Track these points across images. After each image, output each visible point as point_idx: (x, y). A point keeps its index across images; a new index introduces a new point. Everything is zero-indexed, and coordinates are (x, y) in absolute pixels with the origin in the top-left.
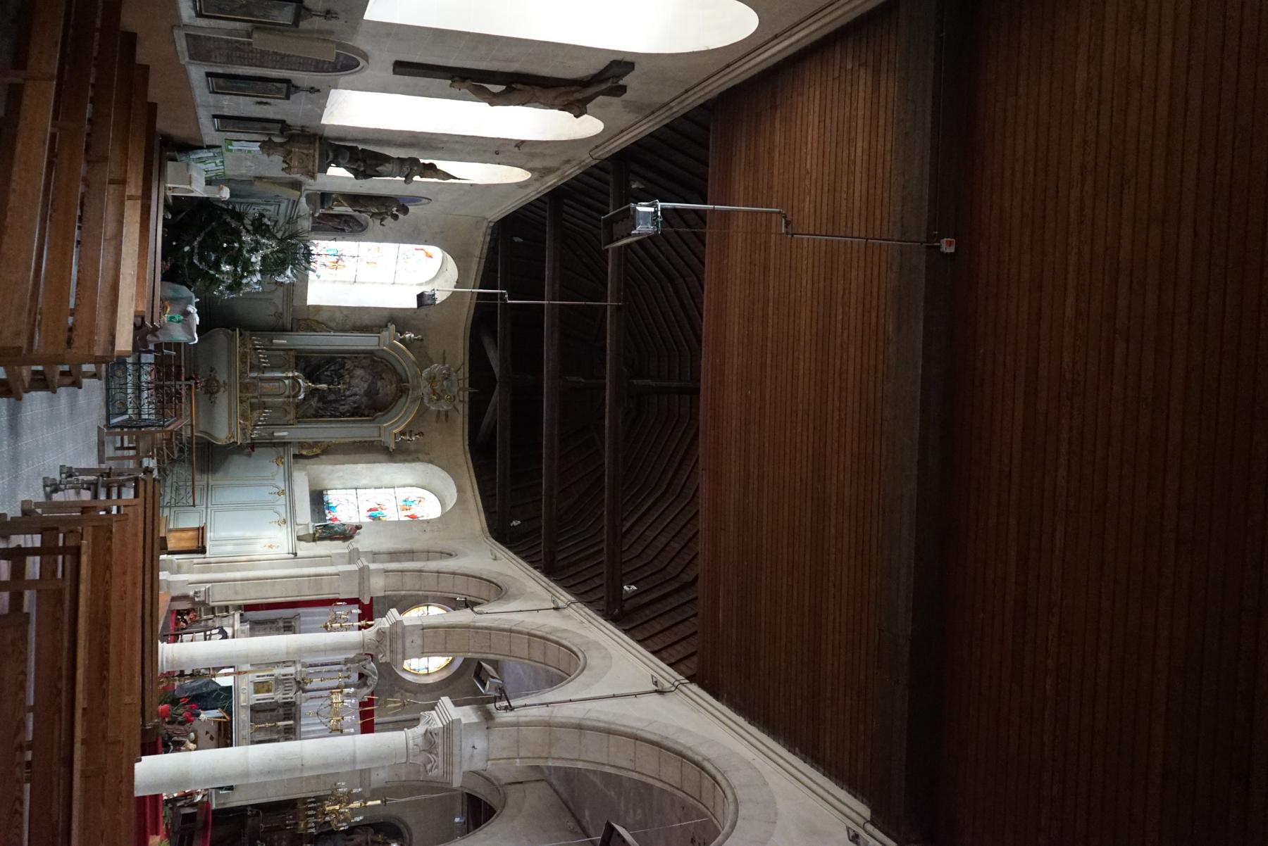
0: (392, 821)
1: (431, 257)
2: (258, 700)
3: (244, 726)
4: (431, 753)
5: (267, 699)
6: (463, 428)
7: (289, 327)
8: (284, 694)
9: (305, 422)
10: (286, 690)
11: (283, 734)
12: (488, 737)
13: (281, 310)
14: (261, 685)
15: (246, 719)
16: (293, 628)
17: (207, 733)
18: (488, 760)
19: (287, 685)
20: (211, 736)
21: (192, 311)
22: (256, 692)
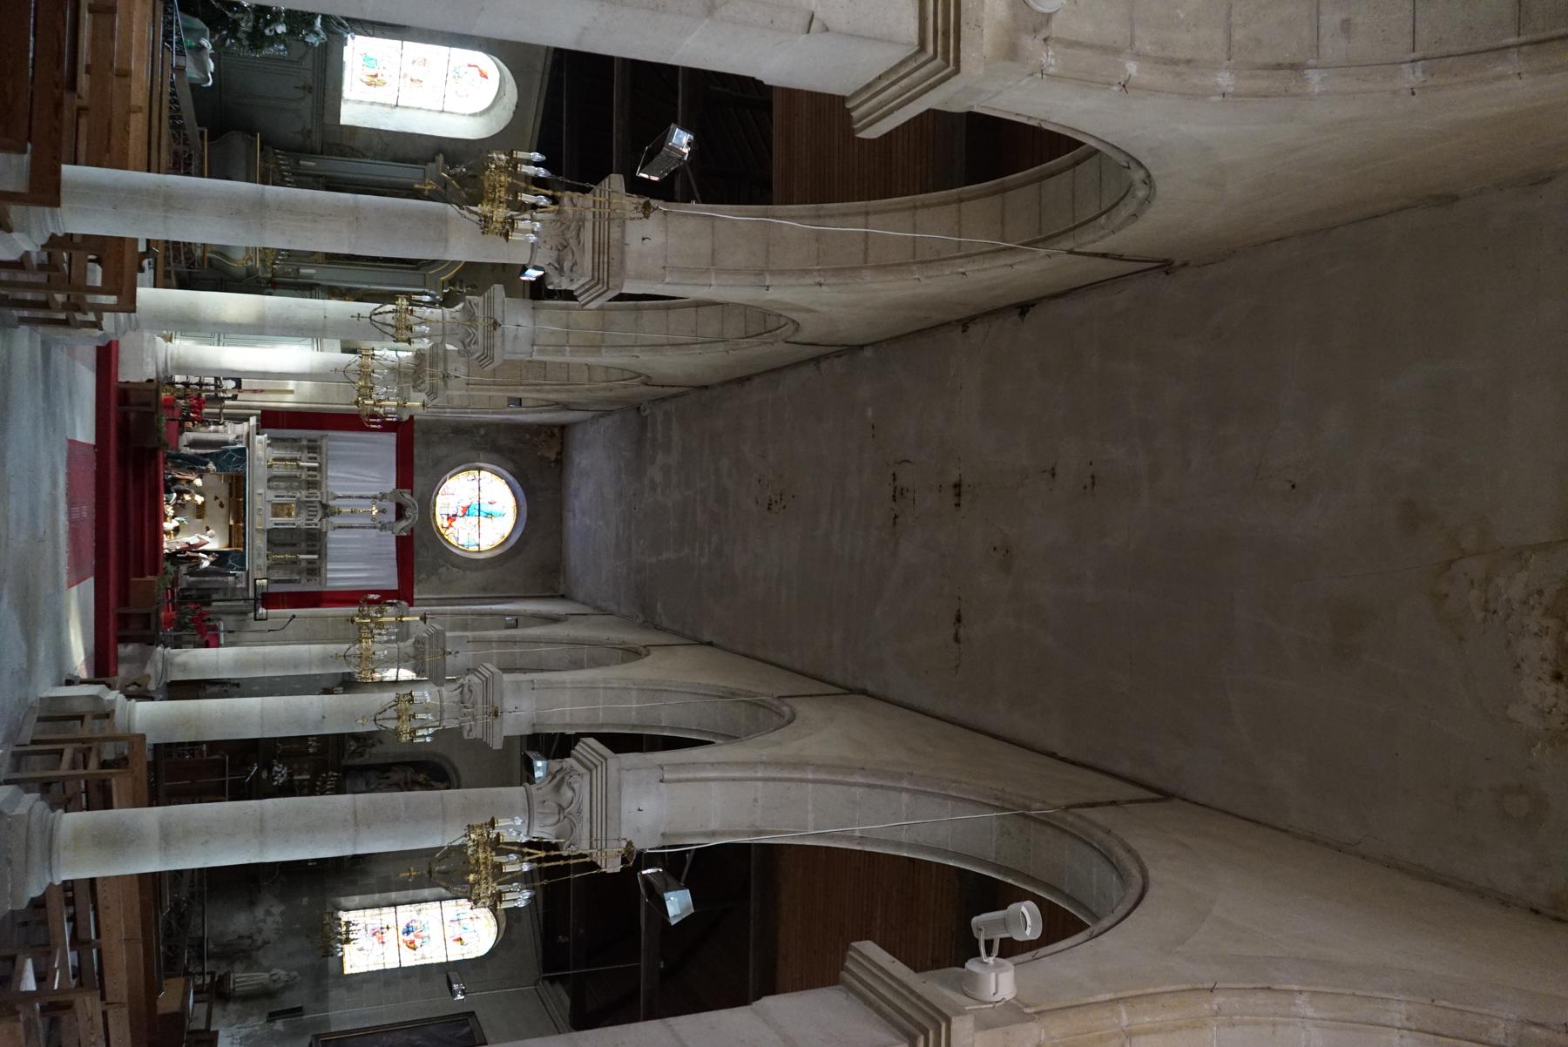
0: (436, 760)
1: (486, 77)
2: (276, 524)
3: (259, 555)
4: (470, 326)
5: (287, 524)
6: (524, 290)
7: (319, 150)
8: (308, 520)
9: (334, 263)
10: (309, 515)
11: (305, 575)
12: (534, 318)
13: (309, 127)
14: (280, 507)
15: (262, 546)
16: (318, 451)
17: (216, 498)
18: (533, 345)
19: (311, 509)
20: (221, 502)
21: (206, 45)
22: (275, 515)
